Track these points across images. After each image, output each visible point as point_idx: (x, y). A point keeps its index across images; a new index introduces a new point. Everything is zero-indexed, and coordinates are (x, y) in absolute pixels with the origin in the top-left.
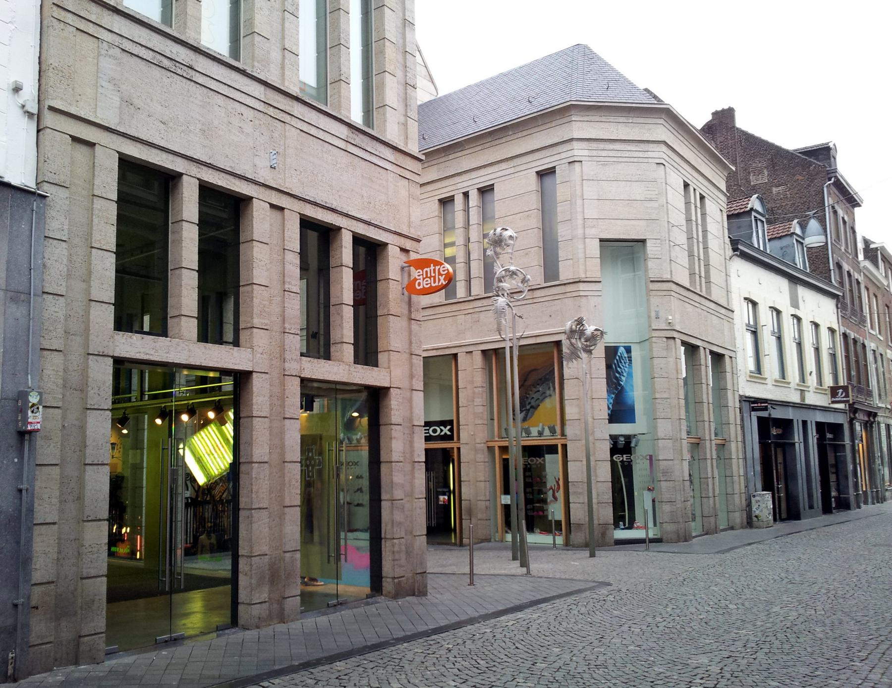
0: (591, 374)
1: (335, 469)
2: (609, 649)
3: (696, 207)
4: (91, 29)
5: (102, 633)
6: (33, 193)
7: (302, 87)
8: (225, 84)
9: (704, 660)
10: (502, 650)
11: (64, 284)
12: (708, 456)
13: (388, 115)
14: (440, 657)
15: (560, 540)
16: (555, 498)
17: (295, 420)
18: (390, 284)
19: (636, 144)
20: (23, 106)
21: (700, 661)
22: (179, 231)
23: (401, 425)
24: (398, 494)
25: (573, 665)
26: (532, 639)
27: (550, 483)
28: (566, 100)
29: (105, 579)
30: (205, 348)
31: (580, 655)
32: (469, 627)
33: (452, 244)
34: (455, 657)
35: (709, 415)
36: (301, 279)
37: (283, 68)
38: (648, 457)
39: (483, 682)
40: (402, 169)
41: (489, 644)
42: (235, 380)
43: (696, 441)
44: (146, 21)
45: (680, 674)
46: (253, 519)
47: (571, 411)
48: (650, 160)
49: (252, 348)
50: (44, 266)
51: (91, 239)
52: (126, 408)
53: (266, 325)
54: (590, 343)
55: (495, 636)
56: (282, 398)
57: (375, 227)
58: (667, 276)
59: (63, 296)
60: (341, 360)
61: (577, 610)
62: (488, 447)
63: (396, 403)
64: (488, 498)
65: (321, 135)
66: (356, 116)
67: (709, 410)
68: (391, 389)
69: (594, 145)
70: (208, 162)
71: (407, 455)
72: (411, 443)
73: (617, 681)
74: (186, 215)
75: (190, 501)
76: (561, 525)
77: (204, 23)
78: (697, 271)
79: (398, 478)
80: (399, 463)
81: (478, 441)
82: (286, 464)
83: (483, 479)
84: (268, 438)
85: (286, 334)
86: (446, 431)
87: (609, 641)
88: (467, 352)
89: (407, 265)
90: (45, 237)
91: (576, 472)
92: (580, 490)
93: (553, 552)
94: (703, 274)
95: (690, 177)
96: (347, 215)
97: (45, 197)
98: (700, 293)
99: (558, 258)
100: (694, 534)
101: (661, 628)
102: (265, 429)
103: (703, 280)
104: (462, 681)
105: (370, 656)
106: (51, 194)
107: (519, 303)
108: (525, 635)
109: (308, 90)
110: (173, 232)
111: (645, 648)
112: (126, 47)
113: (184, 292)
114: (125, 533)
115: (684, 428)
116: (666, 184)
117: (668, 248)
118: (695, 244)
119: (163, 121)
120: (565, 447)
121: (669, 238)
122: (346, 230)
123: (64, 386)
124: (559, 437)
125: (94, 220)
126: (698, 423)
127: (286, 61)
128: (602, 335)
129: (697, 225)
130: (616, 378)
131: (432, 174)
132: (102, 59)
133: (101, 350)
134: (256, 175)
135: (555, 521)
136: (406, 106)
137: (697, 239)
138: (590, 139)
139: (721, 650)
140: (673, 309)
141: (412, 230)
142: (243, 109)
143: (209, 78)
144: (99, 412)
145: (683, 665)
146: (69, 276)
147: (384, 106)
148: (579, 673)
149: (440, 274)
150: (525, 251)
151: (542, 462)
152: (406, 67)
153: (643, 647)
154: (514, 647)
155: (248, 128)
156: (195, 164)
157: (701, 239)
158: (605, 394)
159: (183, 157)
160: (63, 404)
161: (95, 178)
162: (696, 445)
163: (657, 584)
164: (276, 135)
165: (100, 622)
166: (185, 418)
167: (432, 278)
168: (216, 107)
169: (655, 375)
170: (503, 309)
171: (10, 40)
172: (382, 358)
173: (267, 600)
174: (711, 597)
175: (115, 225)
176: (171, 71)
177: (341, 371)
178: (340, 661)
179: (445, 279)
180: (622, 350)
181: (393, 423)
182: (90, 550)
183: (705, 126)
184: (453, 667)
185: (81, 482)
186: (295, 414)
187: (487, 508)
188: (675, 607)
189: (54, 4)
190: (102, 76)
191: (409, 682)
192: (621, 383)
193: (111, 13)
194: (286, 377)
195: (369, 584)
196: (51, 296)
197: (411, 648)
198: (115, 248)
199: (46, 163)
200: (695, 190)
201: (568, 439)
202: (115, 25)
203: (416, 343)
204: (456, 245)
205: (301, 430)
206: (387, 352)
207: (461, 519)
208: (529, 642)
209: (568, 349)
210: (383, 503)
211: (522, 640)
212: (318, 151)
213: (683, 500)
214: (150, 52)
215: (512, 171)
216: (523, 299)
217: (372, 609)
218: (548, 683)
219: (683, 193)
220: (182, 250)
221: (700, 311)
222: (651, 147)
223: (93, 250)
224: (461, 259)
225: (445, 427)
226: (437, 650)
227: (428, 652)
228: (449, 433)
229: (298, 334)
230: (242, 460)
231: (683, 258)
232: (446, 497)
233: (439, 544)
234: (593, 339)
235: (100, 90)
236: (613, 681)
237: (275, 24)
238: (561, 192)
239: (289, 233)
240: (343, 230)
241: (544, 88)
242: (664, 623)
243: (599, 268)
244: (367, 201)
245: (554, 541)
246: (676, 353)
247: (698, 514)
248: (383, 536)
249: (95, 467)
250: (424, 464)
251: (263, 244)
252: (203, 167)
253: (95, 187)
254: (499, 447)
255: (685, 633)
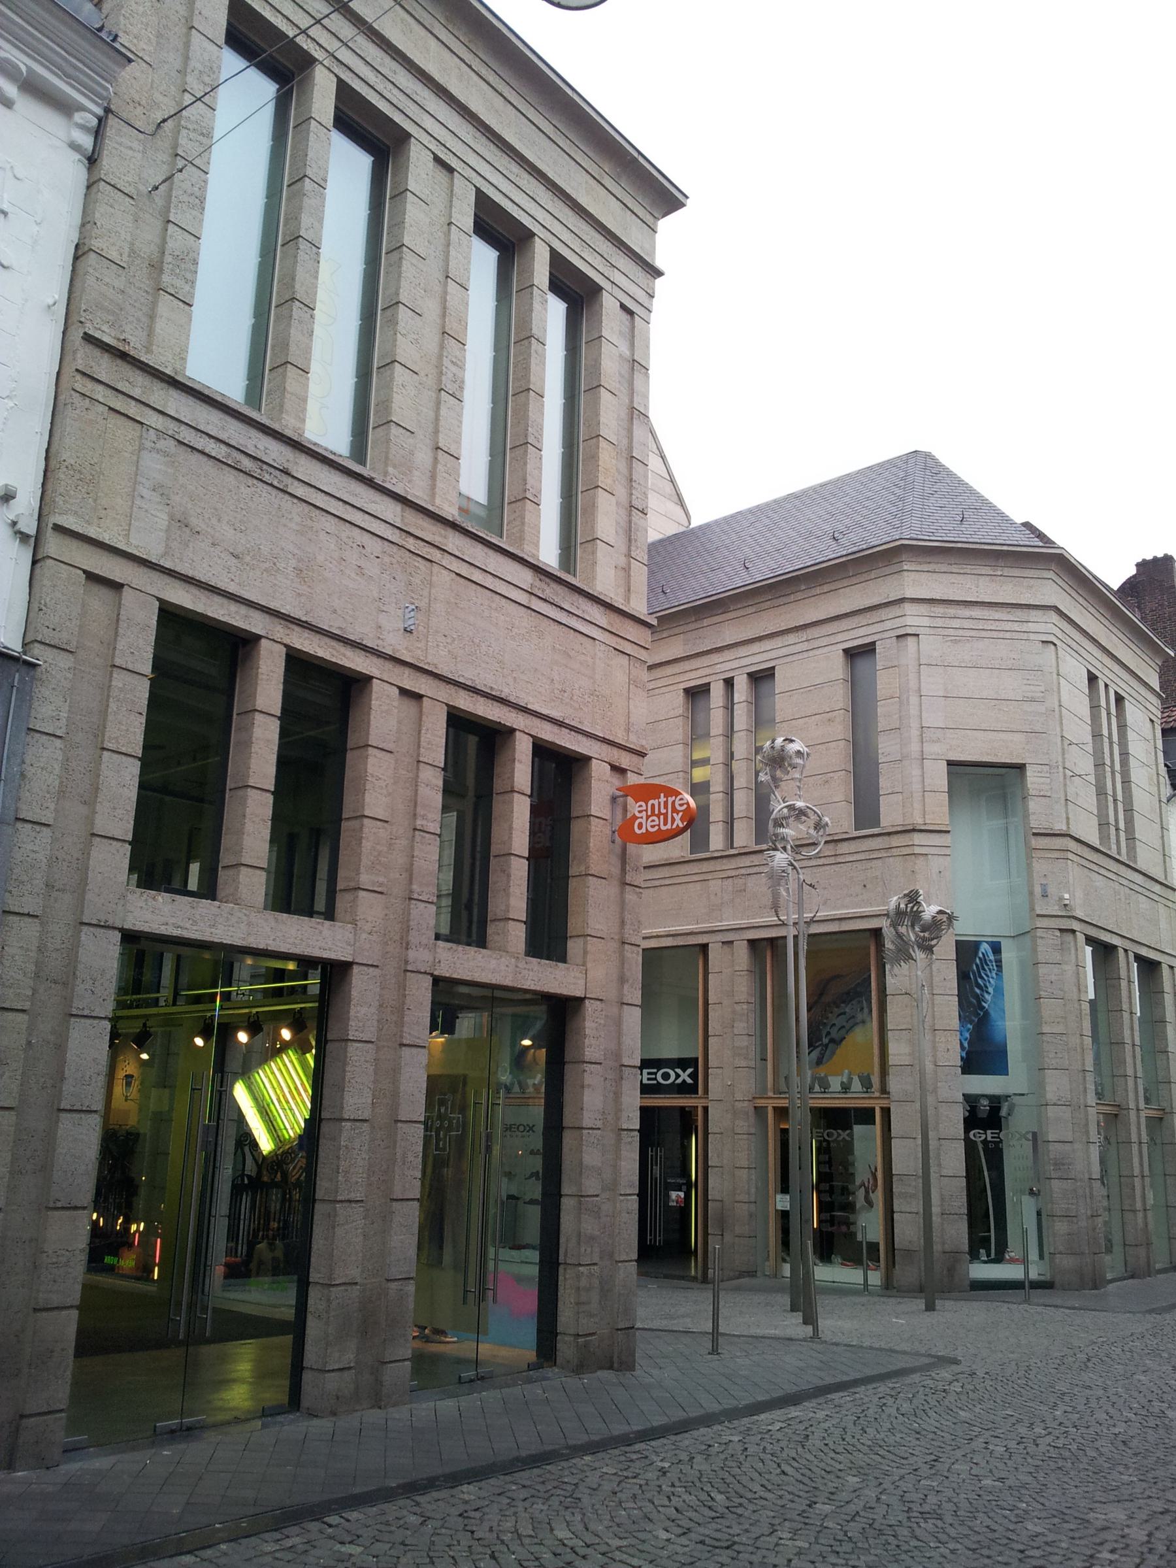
0: (931, 986)
1: (483, 1135)
2: (946, 1483)
3: (1109, 714)
4: (133, 409)
5: (61, 1411)
6: (15, 659)
7: (464, 504)
8: (340, 499)
9: (1118, 1514)
10: (755, 1475)
11: (52, 806)
12: (1134, 1138)
13: (599, 554)
14: (647, 1484)
15: (875, 1278)
16: (870, 1204)
17: (419, 1049)
18: (593, 823)
19: (1009, 610)
20: (14, 524)
21: (1111, 1515)
22: (248, 729)
23: (600, 1064)
24: (591, 1185)
25: (881, 1510)
26: (811, 1458)
27: (861, 1175)
28: (894, 538)
29: (75, 1313)
30: (276, 920)
31: (895, 1492)
32: (703, 1430)
33: (705, 762)
34: (673, 1485)
35: (1135, 1064)
36: (445, 808)
37: (433, 477)
38: (1030, 1136)
39: (718, 1535)
40: (620, 640)
41: (734, 1464)
42: (323, 977)
43: (1114, 1111)
44: (219, 399)
45: (1073, 1538)
46: (338, 1219)
47: (898, 1050)
48: (1032, 636)
49: (354, 923)
50: (23, 775)
51: (103, 736)
52: (147, 1017)
53: (381, 885)
54: (931, 934)
55: (746, 1449)
56: (400, 1010)
57: (571, 730)
58: (1061, 827)
59: (48, 825)
60: (503, 949)
61: (895, 1406)
62: (755, 1108)
63: (594, 1025)
64: (753, 1199)
65: (489, 582)
66: (549, 554)
67: (1134, 1057)
68: (587, 1001)
69: (939, 610)
70: (304, 619)
71: (610, 1118)
72: (617, 1095)
73: (959, 1546)
74: (261, 702)
75: (246, 1181)
76: (879, 1250)
77: (312, 406)
78: (1112, 820)
79: (592, 1157)
80: (595, 1131)
81: (739, 1096)
82: (399, 1125)
83: (745, 1163)
84: (372, 1079)
85: (413, 902)
86: (685, 1076)
87: (947, 1466)
88: (723, 943)
89: (621, 793)
90: (29, 729)
91: (905, 1157)
92: (911, 1191)
93: (864, 1299)
94: (1122, 825)
95: (1099, 666)
96: (525, 710)
97: (34, 666)
98: (1117, 857)
99: (878, 789)
100: (1109, 1276)
101: (1042, 1448)
102: (367, 1062)
103: (1122, 834)
104: (680, 1531)
105: (524, 1477)
106: (45, 662)
107: (814, 863)
108: (800, 1449)
109: (474, 509)
110: (239, 729)
111: (1013, 1485)
112: (184, 438)
113: (249, 827)
114: (135, 1232)
115: (1091, 1087)
116: (1058, 675)
117: (1061, 779)
118: (1109, 775)
119: (236, 553)
120: (886, 1112)
121: (1064, 762)
122: (522, 734)
123: (37, 975)
124: (877, 1094)
125: (111, 705)
126: (1116, 1079)
127: (439, 467)
128: (951, 922)
129: (1111, 743)
130: (977, 997)
131: (674, 648)
132: (144, 454)
133: (103, 918)
134: (380, 642)
135: (867, 1243)
136: (630, 540)
137: (1112, 766)
138: (933, 599)
139: (1150, 1497)
140: (1071, 882)
141: (633, 738)
142: (366, 539)
143: (313, 490)
144: (89, 1021)
145: (1080, 1521)
146: (62, 793)
147: (594, 540)
148: (890, 1526)
149: (674, 810)
150: (824, 777)
151: (848, 1138)
152: (631, 480)
153: (1008, 1483)
154: (778, 1471)
155: (373, 569)
156: (282, 622)
157: (1117, 767)
158: (955, 1023)
159: (263, 611)
160: (32, 1004)
161: (119, 638)
162: (1114, 1118)
163: (1039, 1364)
164: (417, 580)
165: (59, 1391)
166: (243, 1037)
167: (662, 817)
168: (323, 535)
169: (1042, 993)
170: (783, 871)
171: (4, 423)
172: (573, 947)
173: (352, 1365)
174: (1136, 1394)
175: (145, 714)
176: (252, 476)
177: (503, 968)
178: (469, 1483)
179: (682, 820)
180: (985, 947)
181: (587, 1059)
182: (54, 1260)
183: (1125, 583)
184: (667, 1503)
185: (50, 1139)
186: (419, 1038)
187: (751, 1215)
188: (1070, 1409)
189: (77, 370)
190: (144, 481)
191: (587, 1529)
192: (984, 1004)
193: (164, 385)
194: (408, 974)
195: (535, 1348)
196: (29, 826)
197: (597, 1465)
198: (141, 752)
199: (41, 613)
200: (1106, 686)
201: (893, 1099)
202: (169, 404)
203: (632, 924)
204: (711, 762)
205: (428, 1066)
206: (582, 939)
207: (706, 1234)
208: (805, 1462)
209: (893, 942)
210: (564, 1200)
211: (794, 1459)
212: (482, 608)
213: (1089, 1213)
214: (223, 447)
215: (805, 646)
216: (817, 857)
217: (536, 1391)
218: (832, 1542)
219: (1087, 691)
220: (250, 758)
221: (1117, 886)
222: (1034, 615)
223: (105, 753)
224: (717, 786)
225: (684, 1071)
226: (641, 1472)
227: (625, 1474)
228: (689, 1081)
229: (432, 903)
230: (325, 1115)
231: (1089, 799)
232: (682, 1194)
233: (666, 1277)
234: (935, 927)
235: (138, 502)
236: (951, 1546)
237: (425, 410)
238: (885, 683)
239: (429, 736)
240: (517, 733)
241: (858, 518)
242: (1049, 1439)
243: (946, 809)
244: (560, 687)
245: (866, 1279)
246: (1077, 957)
247: (1117, 1238)
248: (561, 1259)
249: (76, 1116)
250: (637, 1134)
251: (384, 753)
252: (294, 627)
253: (117, 652)
254: (775, 1108)
255: (1085, 1460)
